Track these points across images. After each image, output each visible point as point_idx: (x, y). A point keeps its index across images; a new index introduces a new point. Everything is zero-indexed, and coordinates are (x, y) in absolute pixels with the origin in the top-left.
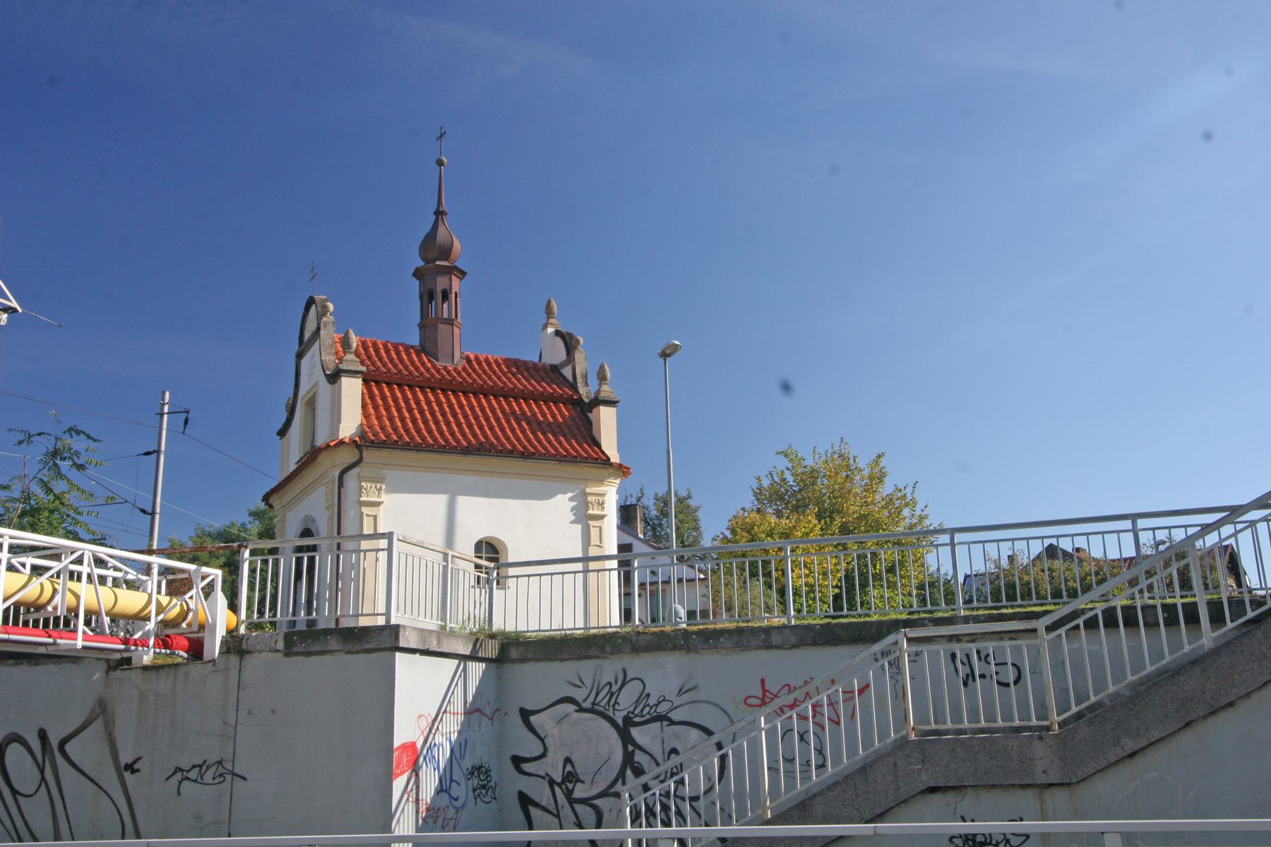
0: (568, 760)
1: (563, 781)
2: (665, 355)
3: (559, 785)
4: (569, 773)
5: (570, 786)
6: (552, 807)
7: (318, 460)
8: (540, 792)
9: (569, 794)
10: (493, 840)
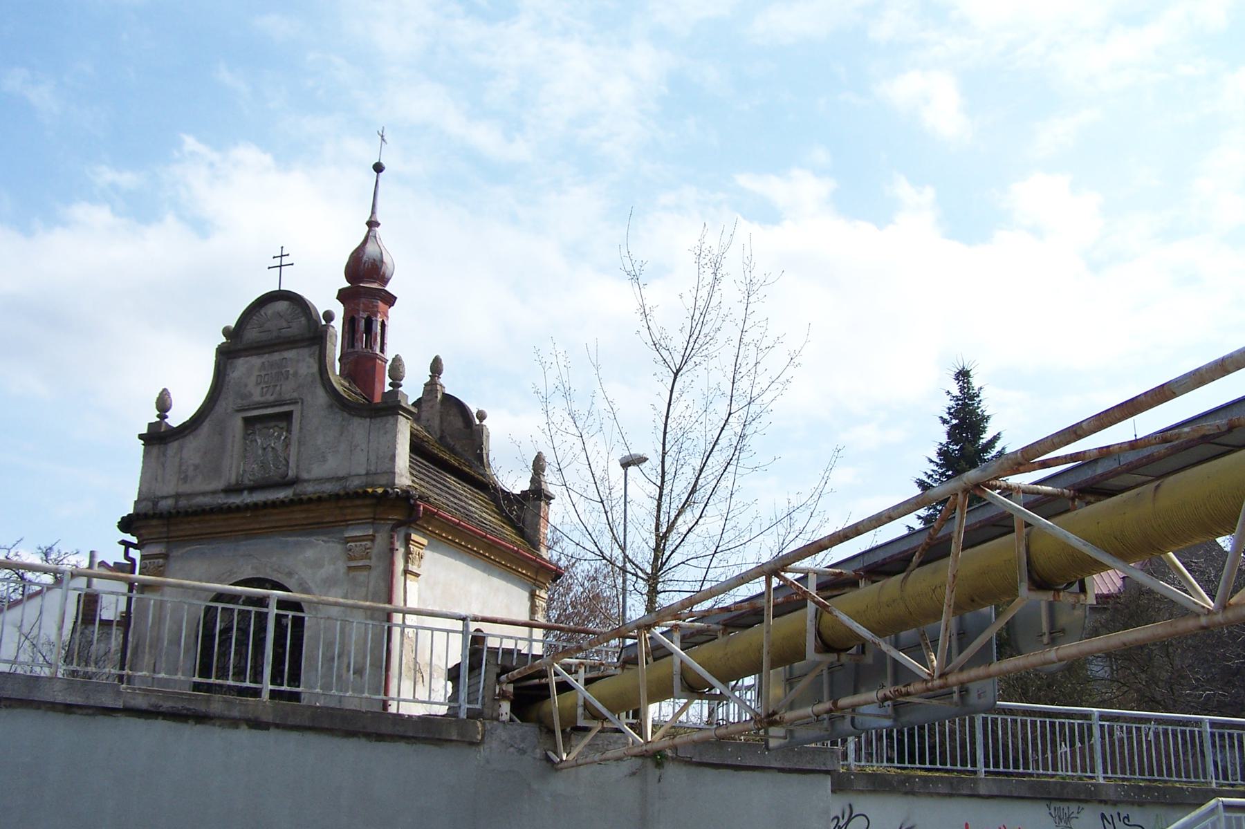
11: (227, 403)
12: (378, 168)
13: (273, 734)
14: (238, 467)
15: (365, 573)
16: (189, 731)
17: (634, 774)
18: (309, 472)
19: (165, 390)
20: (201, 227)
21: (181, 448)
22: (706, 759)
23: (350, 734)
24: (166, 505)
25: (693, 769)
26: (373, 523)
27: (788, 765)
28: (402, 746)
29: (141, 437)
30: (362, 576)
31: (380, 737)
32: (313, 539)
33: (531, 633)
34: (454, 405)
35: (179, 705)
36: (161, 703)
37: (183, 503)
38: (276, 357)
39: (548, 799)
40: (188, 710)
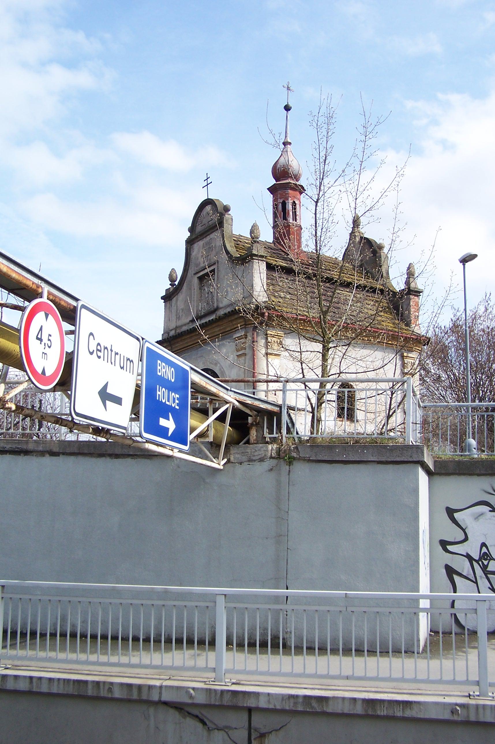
0: (483, 545)
1: (480, 559)
2: (465, 260)
3: (475, 560)
4: (485, 553)
5: (486, 563)
6: (472, 577)
7: (450, 477)
8: (464, 567)
9: (484, 568)
10: (234, 593)
11: (191, 272)
12: (287, 108)
13: (61, 458)
14: (198, 307)
15: (243, 358)
16: (21, 460)
17: (271, 470)
18: (222, 303)
19: (173, 269)
20: (446, 146)
21: (177, 300)
22: (320, 458)
23: (101, 455)
24: (172, 333)
25: (314, 465)
26: (245, 328)
27: (384, 459)
28: (129, 460)
29: (162, 298)
30: (242, 359)
31: (117, 456)
32: (224, 342)
33: (268, 386)
34: (368, 243)
35: (14, 446)
36: (5, 446)
37: (179, 331)
38: (208, 238)
39: (216, 488)
40: (18, 448)
